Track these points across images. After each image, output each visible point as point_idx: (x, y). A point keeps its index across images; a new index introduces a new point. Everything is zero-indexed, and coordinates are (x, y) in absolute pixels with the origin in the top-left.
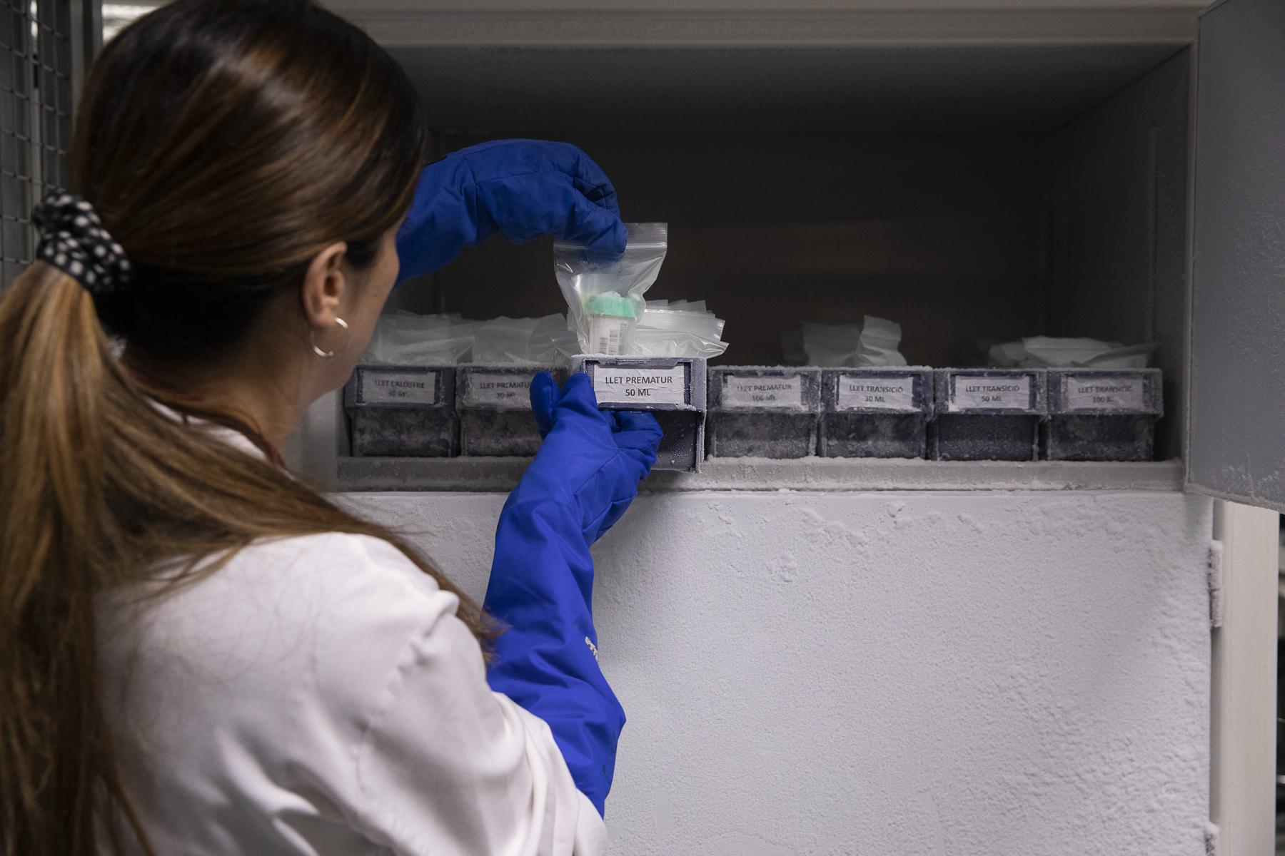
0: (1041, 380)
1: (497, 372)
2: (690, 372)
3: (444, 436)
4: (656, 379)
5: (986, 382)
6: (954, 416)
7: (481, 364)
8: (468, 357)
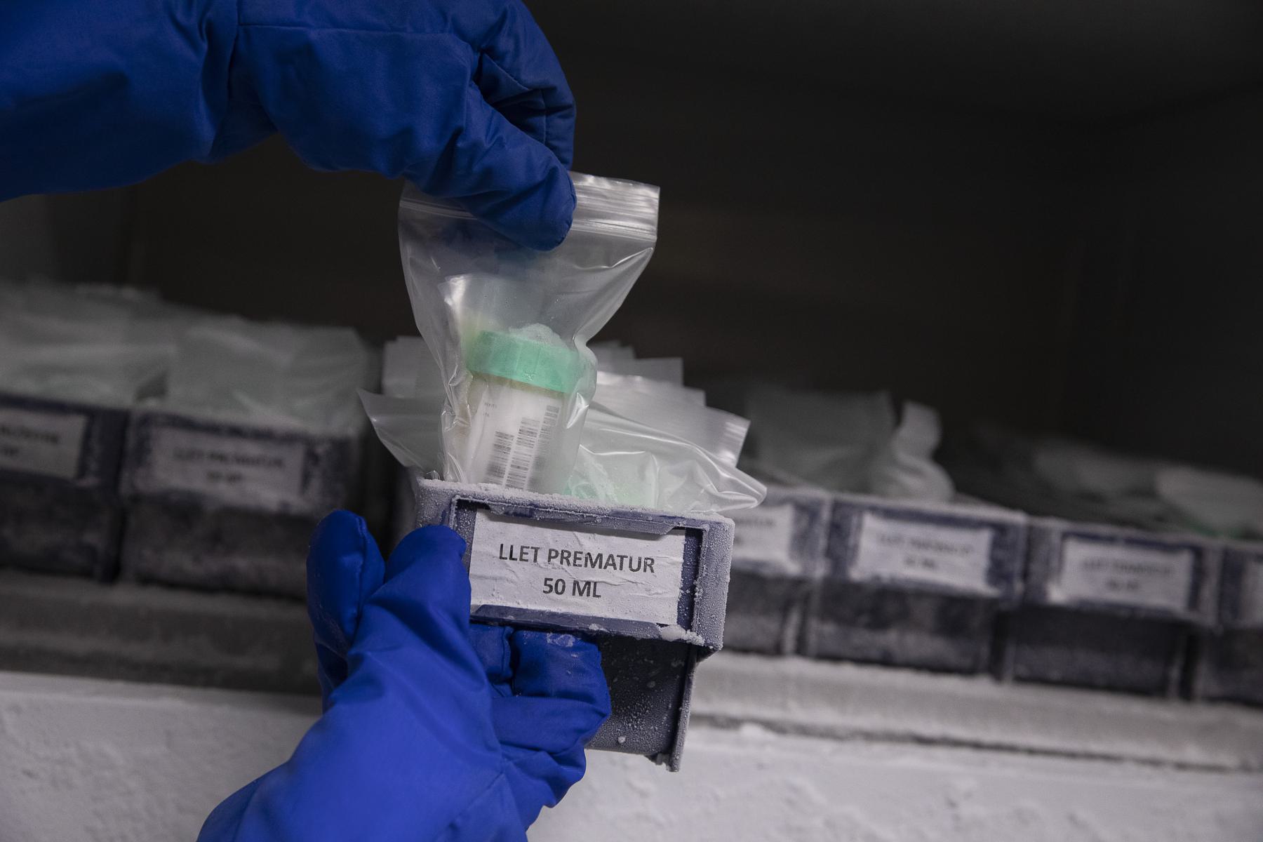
0: (1213, 563)
1: (213, 429)
2: (698, 551)
4: (617, 561)
5: (1118, 554)
6: (1059, 612)
7: (184, 410)
8: (157, 388)
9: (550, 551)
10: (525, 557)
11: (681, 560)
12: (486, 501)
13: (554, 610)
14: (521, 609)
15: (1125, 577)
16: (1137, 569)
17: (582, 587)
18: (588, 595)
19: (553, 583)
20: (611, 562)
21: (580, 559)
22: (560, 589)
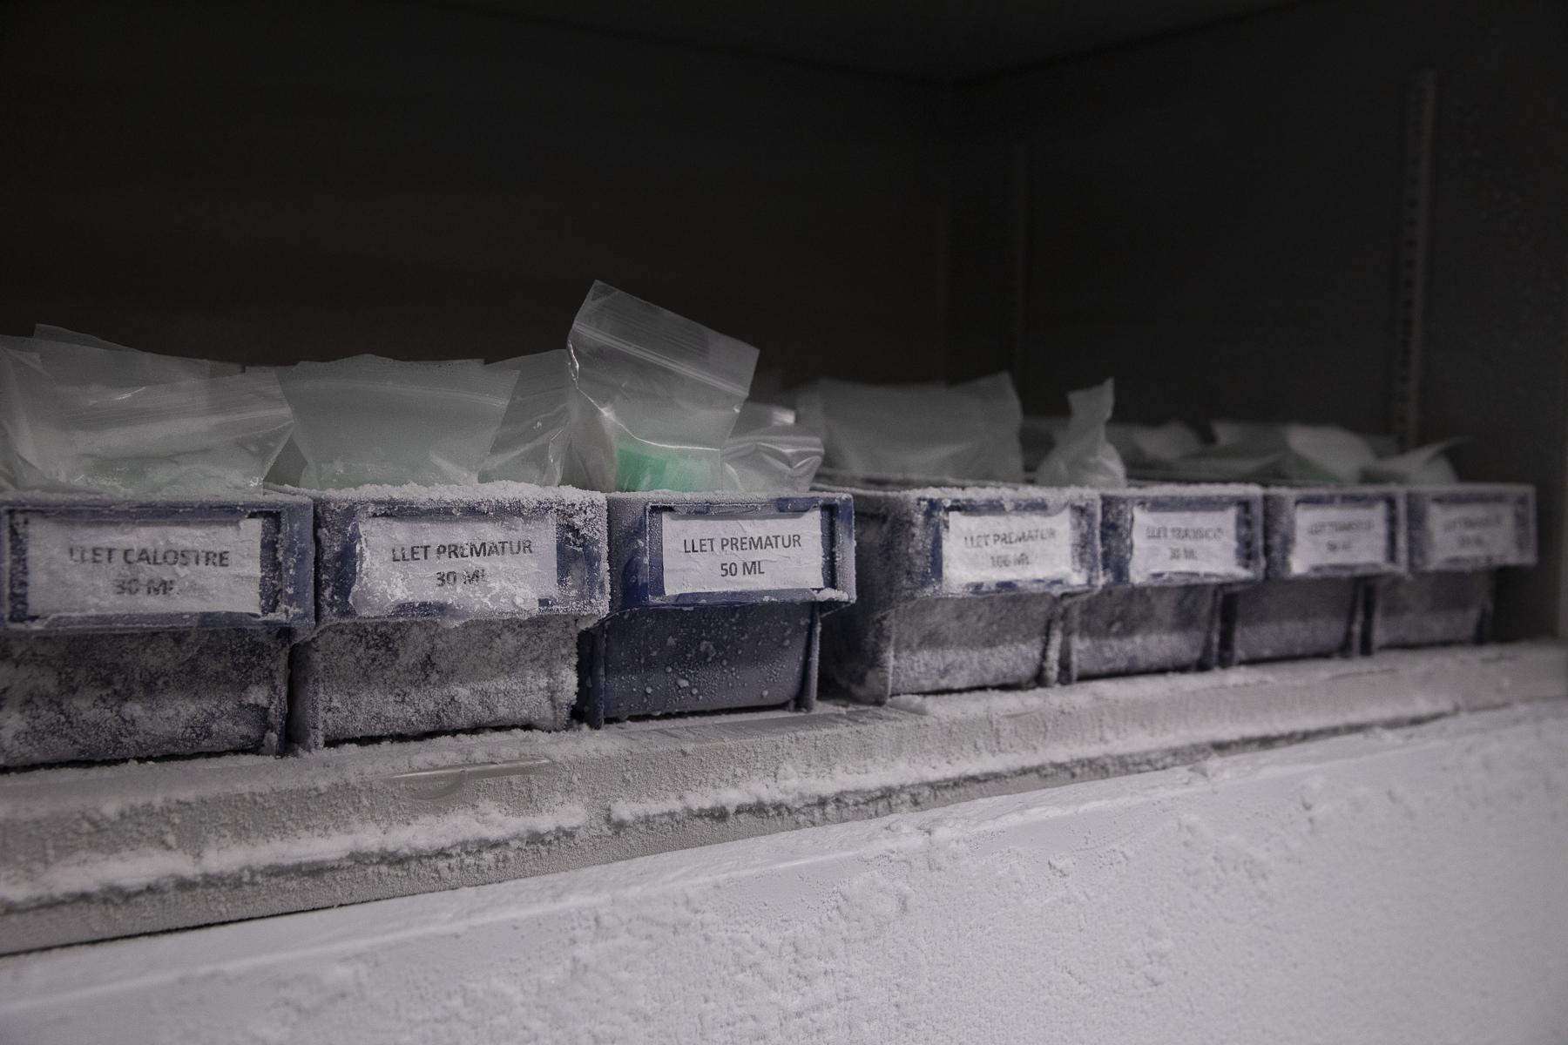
0: (1402, 507)
3: (258, 695)
9: (722, 540)
10: (704, 548)
11: (820, 533)
12: (673, 505)
13: (732, 589)
14: (709, 593)
15: (1340, 537)
16: (1347, 527)
17: (749, 566)
18: (755, 573)
19: (727, 567)
20: (768, 542)
21: (705, 545)
22: (733, 572)
